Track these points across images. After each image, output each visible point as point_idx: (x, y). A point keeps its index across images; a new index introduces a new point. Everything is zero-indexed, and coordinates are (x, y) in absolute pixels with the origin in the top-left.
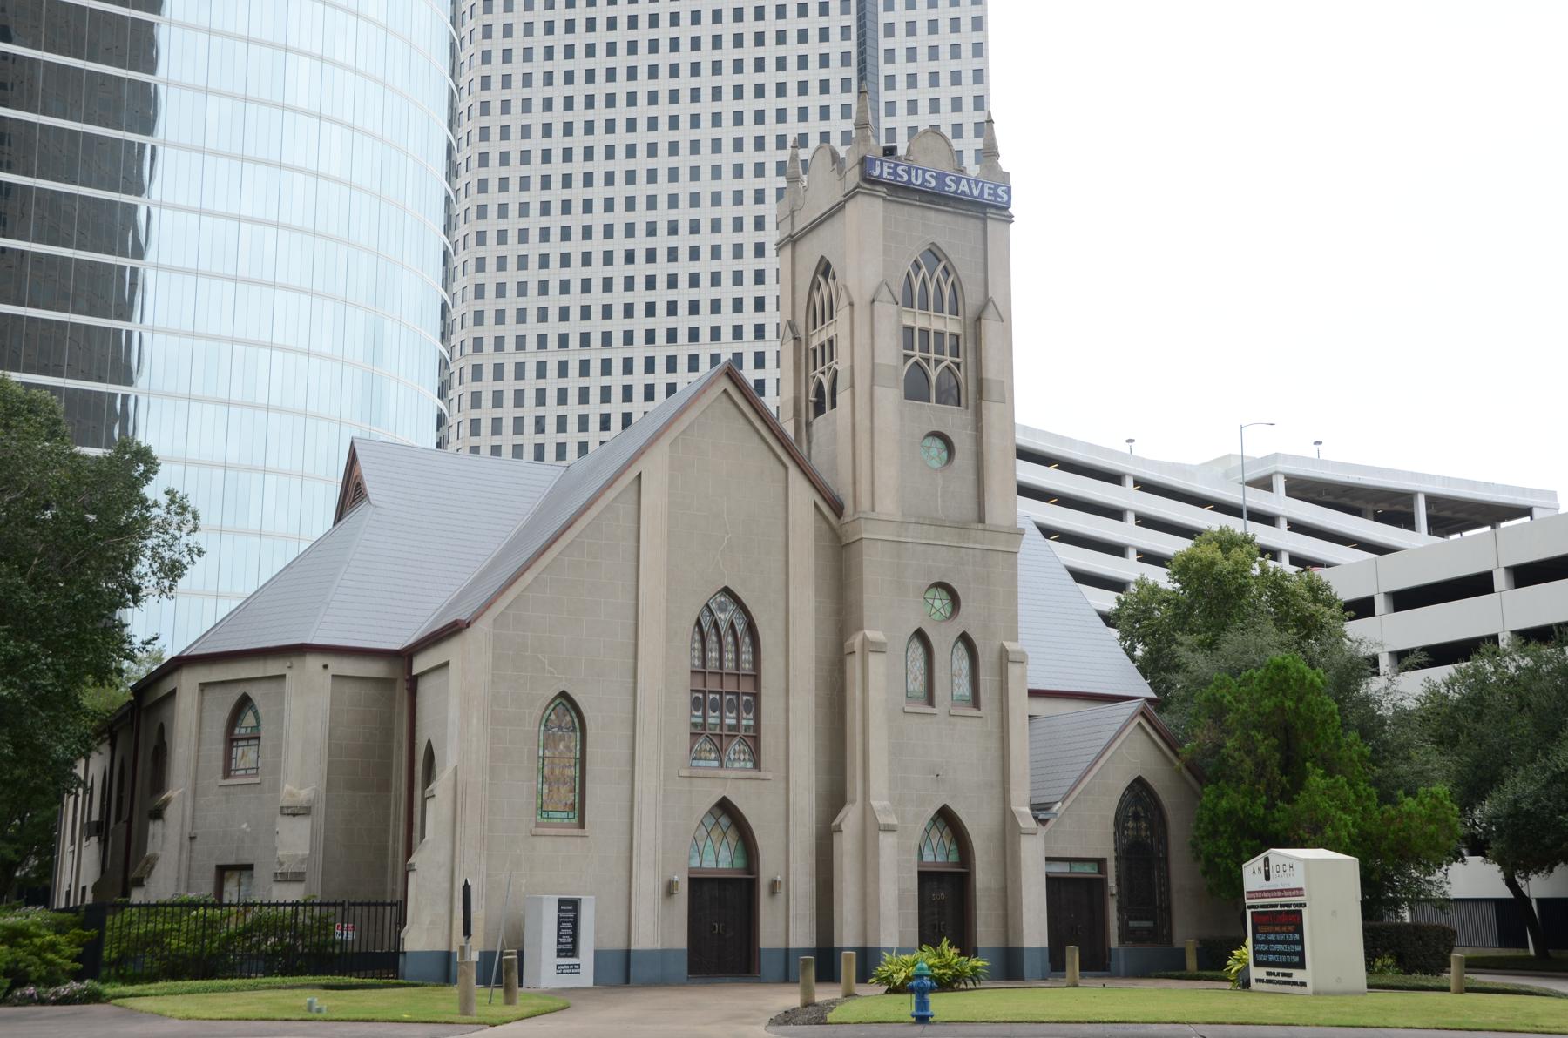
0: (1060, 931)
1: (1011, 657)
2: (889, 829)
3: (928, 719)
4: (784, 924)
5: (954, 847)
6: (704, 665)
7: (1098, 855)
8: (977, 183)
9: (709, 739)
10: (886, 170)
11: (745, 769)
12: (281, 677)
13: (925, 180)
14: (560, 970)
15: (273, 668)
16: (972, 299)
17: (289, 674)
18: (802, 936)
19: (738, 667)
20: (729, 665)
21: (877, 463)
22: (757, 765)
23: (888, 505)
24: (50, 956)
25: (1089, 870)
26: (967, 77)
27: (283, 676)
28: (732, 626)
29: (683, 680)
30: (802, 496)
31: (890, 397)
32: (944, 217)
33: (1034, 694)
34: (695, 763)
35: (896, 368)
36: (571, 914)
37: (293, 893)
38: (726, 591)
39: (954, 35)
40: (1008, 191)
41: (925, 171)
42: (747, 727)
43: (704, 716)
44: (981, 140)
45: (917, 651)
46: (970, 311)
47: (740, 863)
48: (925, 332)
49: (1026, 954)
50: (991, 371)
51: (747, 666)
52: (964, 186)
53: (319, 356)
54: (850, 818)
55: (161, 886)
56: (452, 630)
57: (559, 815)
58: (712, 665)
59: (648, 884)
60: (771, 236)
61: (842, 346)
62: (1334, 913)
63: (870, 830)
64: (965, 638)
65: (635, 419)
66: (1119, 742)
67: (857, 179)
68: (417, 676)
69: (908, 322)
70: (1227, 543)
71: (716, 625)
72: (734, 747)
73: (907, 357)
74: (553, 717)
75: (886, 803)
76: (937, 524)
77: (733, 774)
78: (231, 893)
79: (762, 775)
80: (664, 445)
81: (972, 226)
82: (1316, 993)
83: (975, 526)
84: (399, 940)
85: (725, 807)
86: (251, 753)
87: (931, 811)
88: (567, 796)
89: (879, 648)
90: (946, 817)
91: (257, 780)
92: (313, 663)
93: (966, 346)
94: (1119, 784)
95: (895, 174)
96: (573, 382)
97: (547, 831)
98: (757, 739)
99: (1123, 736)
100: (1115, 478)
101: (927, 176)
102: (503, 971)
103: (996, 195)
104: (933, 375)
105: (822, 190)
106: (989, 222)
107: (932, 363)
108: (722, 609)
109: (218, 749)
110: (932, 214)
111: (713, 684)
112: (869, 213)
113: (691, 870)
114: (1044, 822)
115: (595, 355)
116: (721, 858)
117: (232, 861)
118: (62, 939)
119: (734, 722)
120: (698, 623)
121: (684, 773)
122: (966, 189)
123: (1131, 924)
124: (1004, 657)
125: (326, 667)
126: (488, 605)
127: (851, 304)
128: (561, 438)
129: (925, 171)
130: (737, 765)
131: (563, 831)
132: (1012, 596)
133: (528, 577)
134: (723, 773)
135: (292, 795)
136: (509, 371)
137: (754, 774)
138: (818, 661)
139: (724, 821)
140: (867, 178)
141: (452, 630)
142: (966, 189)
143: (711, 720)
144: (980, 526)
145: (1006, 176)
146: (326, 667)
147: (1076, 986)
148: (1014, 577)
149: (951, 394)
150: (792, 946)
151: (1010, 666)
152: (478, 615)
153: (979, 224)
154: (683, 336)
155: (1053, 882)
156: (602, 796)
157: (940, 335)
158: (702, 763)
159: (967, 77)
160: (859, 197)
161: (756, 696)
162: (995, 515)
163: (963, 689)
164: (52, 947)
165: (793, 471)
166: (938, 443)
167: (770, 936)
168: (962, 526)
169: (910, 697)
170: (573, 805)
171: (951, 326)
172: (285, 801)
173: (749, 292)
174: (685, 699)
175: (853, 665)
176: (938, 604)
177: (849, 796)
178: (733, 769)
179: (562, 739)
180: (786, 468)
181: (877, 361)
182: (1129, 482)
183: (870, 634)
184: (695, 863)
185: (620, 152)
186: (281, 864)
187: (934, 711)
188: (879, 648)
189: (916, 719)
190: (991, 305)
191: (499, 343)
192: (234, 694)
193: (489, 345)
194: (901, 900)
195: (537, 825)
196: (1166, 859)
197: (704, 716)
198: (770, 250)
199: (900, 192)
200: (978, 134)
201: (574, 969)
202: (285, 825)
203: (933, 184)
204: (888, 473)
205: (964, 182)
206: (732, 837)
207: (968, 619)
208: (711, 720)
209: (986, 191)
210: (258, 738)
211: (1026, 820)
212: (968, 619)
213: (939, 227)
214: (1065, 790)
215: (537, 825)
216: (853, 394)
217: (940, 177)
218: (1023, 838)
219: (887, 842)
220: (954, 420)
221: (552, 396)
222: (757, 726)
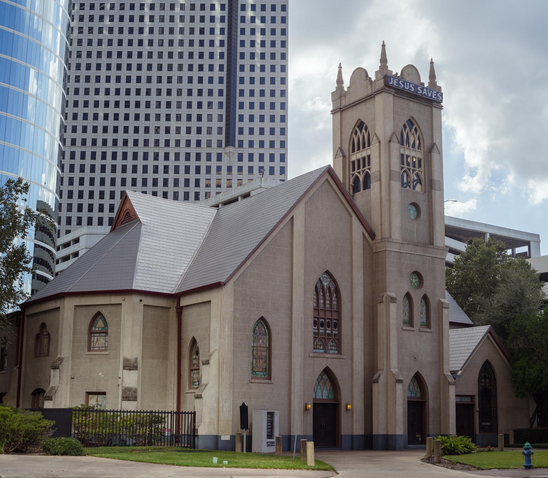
0: (464, 428)
1: (444, 305)
3: (411, 333)
4: (352, 424)
5: (418, 390)
8: (430, 90)
9: (320, 340)
10: (395, 82)
11: (334, 354)
13: (410, 88)
15: (115, 300)
17: (123, 303)
18: (358, 430)
19: (331, 307)
22: (340, 352)
23: (396, 235)
25: (467, 400)
26: (278, 32)
27: (121, 304)
28: (329, 288)
29: (311, 313)
30: (358, 229)
32: (416, 105)
38: (327, 272)
39: (273, 12)
40: (442, 95)
41: (410, 84)
42: (335, 334)
43: (318, 329)
47: (331, 397)
49: (312, 439)
50: (436, 177)
51: (335, 307)
56: (218, 286)
57: (260, 373)
58: (321, 306)
61: (374, 161)
67: (383, 85)
68: (182, 307)
69: (402, 152)
71: (323, 288)
73: (402, 168)
76: (416, 244)
80: (302, 204)
81: (427, 109)
83: (430, 246)
85: (327, 371)
86: (102, 341)
87: (412, 374)
88: (262, 364)
89: (393, 300)
90: (418, 378)
91: (107, 353)
92: (136, 299)
95: (398, 84)
96: (130, 162)
97: (256, 381)
101: (411, 87)
106: (434, 109)
107: (411, 171)
110: (411, 104)
111: (322, 314)
115: (141, 150)
116: (324, 394)
119: (329, 332)
121: (311, 355)
122: (426, 93)
123: (483, 424)
125: (141, 301)
126: (232, 275)
127: (380, 142)
128: (81, 188)
129: (410, 84)
130: (331, 352)
133: (248, 263)
134: (327, 356)
136: (99, 155)
137: (339, 356)
140: (387, 85)
141: (218, 286)
142: (426, 93)
143: (321, 331)
145: (440, 88)
146: (141, 301)
147: (502, 451)
152: (228, 280)
153: (429, 108)
155: (458, 405)
158: (317, 351)
159: (278, 32)
160: (383, 94)
165: (354, 218)
166: (414, 208)
167: (345, 430)
174: (311, 321)
175: (381, 308)
177: (379, 367)
178: (330, 353)
179: (260, 338)
180: (351, 216)
185: (135, 55)
188: (393, 300)
189: (407, 332)
190: (435, 147)
191: (105, 142)
195: (252, 378)
196: (496, 396)
204: (396, 221)
206: (328, 384)
210: (107, 333)
213: (414, 109)
215: (252, 378)
216: (381, 183)
217: (416, 87)
221: (77, 168)
222: (339, 335)
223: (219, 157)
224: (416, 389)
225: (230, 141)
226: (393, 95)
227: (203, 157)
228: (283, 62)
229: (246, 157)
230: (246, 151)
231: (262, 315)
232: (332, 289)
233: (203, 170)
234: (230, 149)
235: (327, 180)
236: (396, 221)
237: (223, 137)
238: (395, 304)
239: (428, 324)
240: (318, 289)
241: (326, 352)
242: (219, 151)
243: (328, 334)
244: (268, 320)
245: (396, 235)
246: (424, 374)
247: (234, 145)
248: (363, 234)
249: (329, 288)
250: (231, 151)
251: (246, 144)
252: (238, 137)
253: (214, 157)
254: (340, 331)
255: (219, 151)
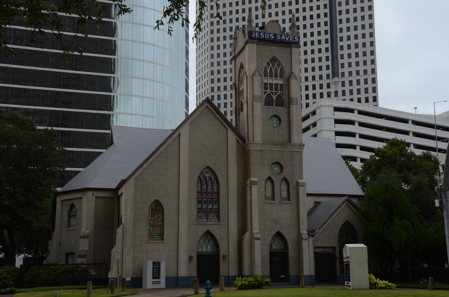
1: (300, 184)
2: (258, 239)
4: (228, 268)
5: (283, 244)
6: (201, 190)
7: (332, 246)
10: (257, 34)
11: (215, 221)
12: (81, 198)
14: (154, 283)
15: (79, 195)
16: (287, 72)
17: (83, 197)
20: (210, 190)
21: (254, 126)
22: (219, 220)
23: (258, 139)
24: (4, 281)
25: (330, 250)
27: (82, 197)
28: (210, 178)
31: (258, 106)
33: (308, 195)
34: (199, 220)
35: (261, 96)
36: (158, 266)
37: (84, 260)
38: (208, 167)
41: (270, 34)
42: (216, 209)
43: (202, 206)
44: (290, 24)
45: (269, 184)
46: (286, 77)
48: (271, 84)
52: (283, 37)
53: (146, 98)
54: (247, 236)
55: (51, 259)
57: (156, 237)
59: (183, 257)
60: (228, 58)
62: (359, 264)
63: (252, 239)
64: (285, 179)
65: (310, 105)
66: (339, 210)
69: (265, 81)
70: (393, 143)
71: (205, 178)
72: (211, 215)
73: (265, 93)
74: (154, 207)
75: (258, 231)
76: (275, 144)
77: (210, 223)
78: (70, 262)
79: (220, 223)
80: (187, 124)
81: (287, 50)
82: (353, 289)
83: (287, 144)
84: (107, 275)
85: (208, 233)
87: (274, 233)
89: (255, 183)
90: (279, 235)
91: (76, 228)
92: (90, 194)
93: (285, 88)
94: (340, 223)
98: (218, 212)
99: (341, 208)
100: (405, 121)
101: (271, 35)
102: (137, 282)
103: (294, 39)
104: (274, 98)
105: (241, 41)
106: (293, 49)
107: (274, 94)
108: (207, 173)
109: (65, 219)
110: (273, 47)
111: (204, 196)
112: (252, 49)
113: (198, 252)
114: (313, 236)
116: (207, 248)
117: (69, 251)
118: (9, 276)
119: (211, 207)
120: (199, 177)
121: (195, 223)
122: (284, 38)
124: (298, 185)
125: (93, 194)
127: (247, 77)
130: (212, 220)
131: (156, 241)
132: (301, 165)
133: (145, 166)
134: (207, 223)
135: (83, 232)
136: (222, 97)
138: (238, 188)
139: (209, 237)
140: (250, 37)
144: (289, 144)
146: (93, 194)
148: (301, 160)
149: (280, 103)
150: (230, 275)
151: (300, 187)
153: (289, 49)
154: (362, 73)
155: (317, 255)
156: (169, 231)
157: (276, 85)
158: (201, 220)
161: (218, 199)
162: (295, 140)
163: (285, 194)
164: (5, 278)
165: (229, 130)
166: (276, 119)
167: (223, 272)
168: (283, 144)
169: (266, 198)
170: (160, 233)
171: (280, 82)
172: (82, 234)
173: (310, 65)
174: (195, 201)
175: (248, 188)
176: (276, 169)
180: (227, 129)
181: (254, 94)
182: (410, 122)
183: (252, 179)
184: (200, 250)
186: (80, 252)
187: (275, 202)
190: (293, 74)
191: (219, 88)
192: (70, 203)
193: (216, 89)
194: (263, 261)
195: (149, 240)
197: (202, 206)
198: (228, 62)
199: (261, 41)
200: (290, 21)
201: (159, 283)
202: (81, 241)
203: (273, 37)
204: (258, 130)
205: (283, 36)
207: (286, 173)
208: (204, 207)
209: (291, 38)
211: (305, 236)
212: (286, 173)
213: (276, 51)
214: (320, 226)
215: (149, 240)
217: (275, 35)
218: (303, 241)
219: (257, 244)
220: (281, 111)
222: (219, 208)
223: (328, 86)
224: (281, 243)
225: (335, 74)
226: (257, 44)
227: (318, 87)
228: (370, 12)
229: (347, 83)
230: (347, 79)
231: (156, 198)
232: (213, 179)
233: (311, 96)
234: (336, 79)
235: (207, 106)
236: (258, 130)
237: (330, 72)
238: (256, 186)
239: (289, 199)
240: (201, 180)
241: (207, 221)
242: (328, 81)
243: (210, 208)
244: (161, 201)
245: (258, 139)
246: (284, 233)
247: (338, 76)
248: (237, 139)
249: (210, 178)
250: (336, 80)
251: (347, 74)
252: (341, 70)
253: (325, 86)
254: (219, 206)
255: (328, 81)
